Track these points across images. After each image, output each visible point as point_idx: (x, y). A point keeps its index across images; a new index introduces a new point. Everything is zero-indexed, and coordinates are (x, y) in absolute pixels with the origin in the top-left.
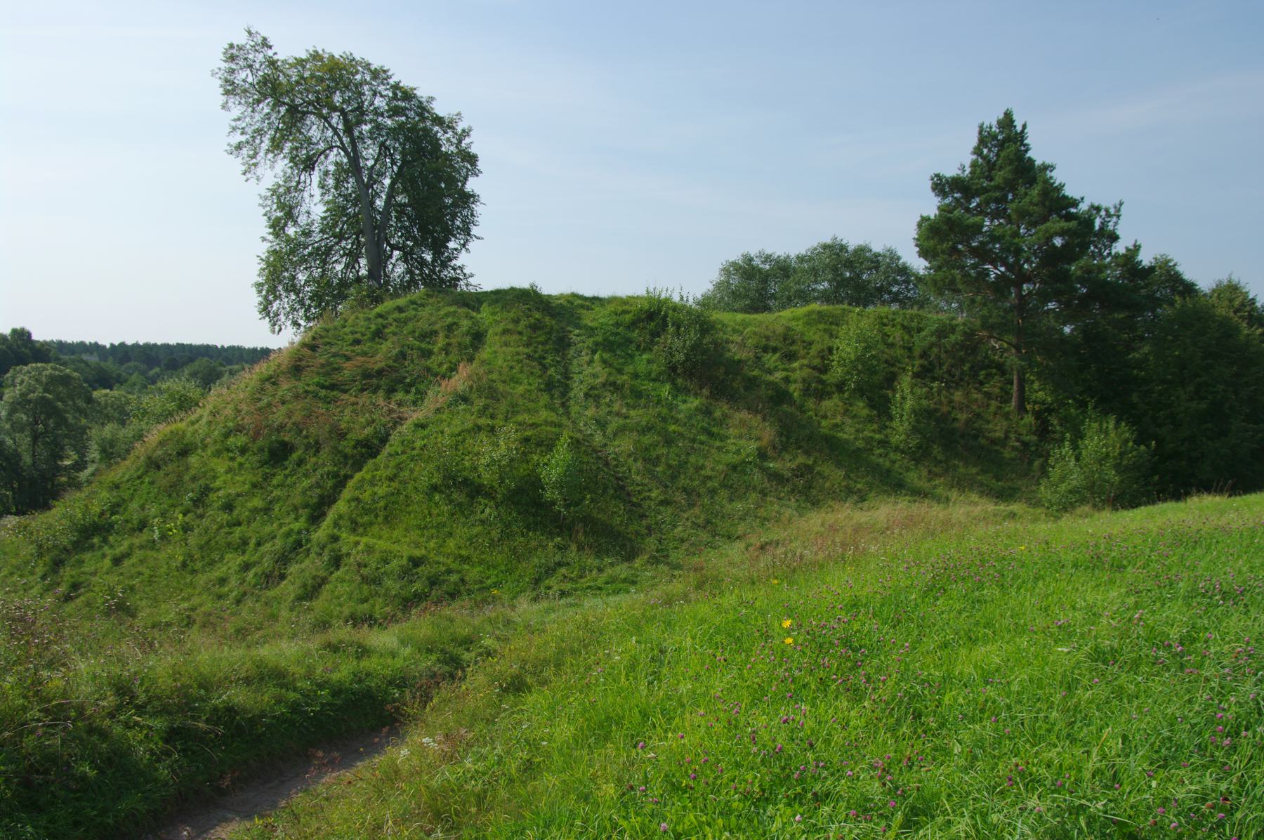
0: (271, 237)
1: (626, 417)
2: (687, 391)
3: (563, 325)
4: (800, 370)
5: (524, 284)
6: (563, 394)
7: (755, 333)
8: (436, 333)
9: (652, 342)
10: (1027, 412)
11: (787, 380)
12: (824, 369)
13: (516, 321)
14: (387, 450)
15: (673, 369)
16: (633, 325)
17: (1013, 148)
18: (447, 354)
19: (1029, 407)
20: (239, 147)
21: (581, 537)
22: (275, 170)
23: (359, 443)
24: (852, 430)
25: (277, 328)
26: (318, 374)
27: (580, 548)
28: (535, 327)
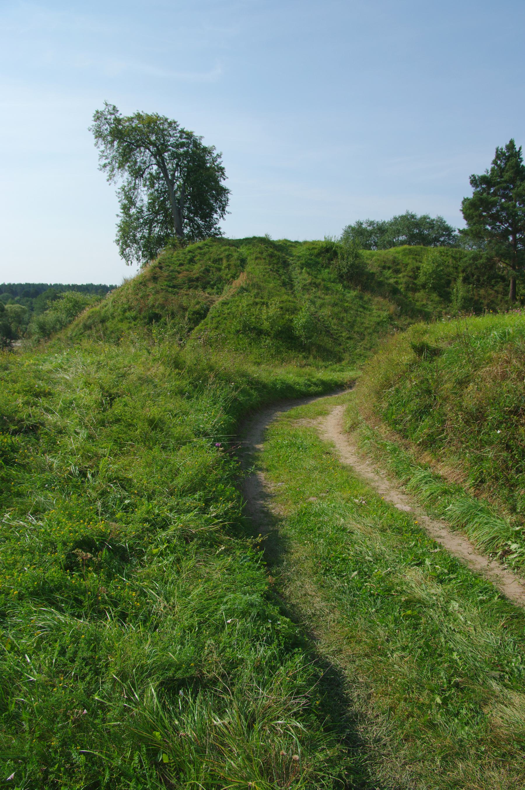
0: (122, 215)
1: (324, 299)
2: (349, 287)
3: (284, 255)
4: (402, 278)
5: (262, 235)
6: (291, 289)
7: (378, 260)
8: (221, 259)
9: (329, 264)
10: (516, 300)
11: (397, 283)
12: (415, 277)
13: (261, 253)
14: (209, 316)
15: (342, 276)
16: (319, 255)
17: (514, 160)
18: (229, 270)
19: (518, 298)
20: (105, 166)
21: (315, 353)
22: (123, 178)
23: (195, 313)
24: (432, 307)
25: (130, 262)
26: (166, 280)
27: (315, 357)
28: (271, 256)
